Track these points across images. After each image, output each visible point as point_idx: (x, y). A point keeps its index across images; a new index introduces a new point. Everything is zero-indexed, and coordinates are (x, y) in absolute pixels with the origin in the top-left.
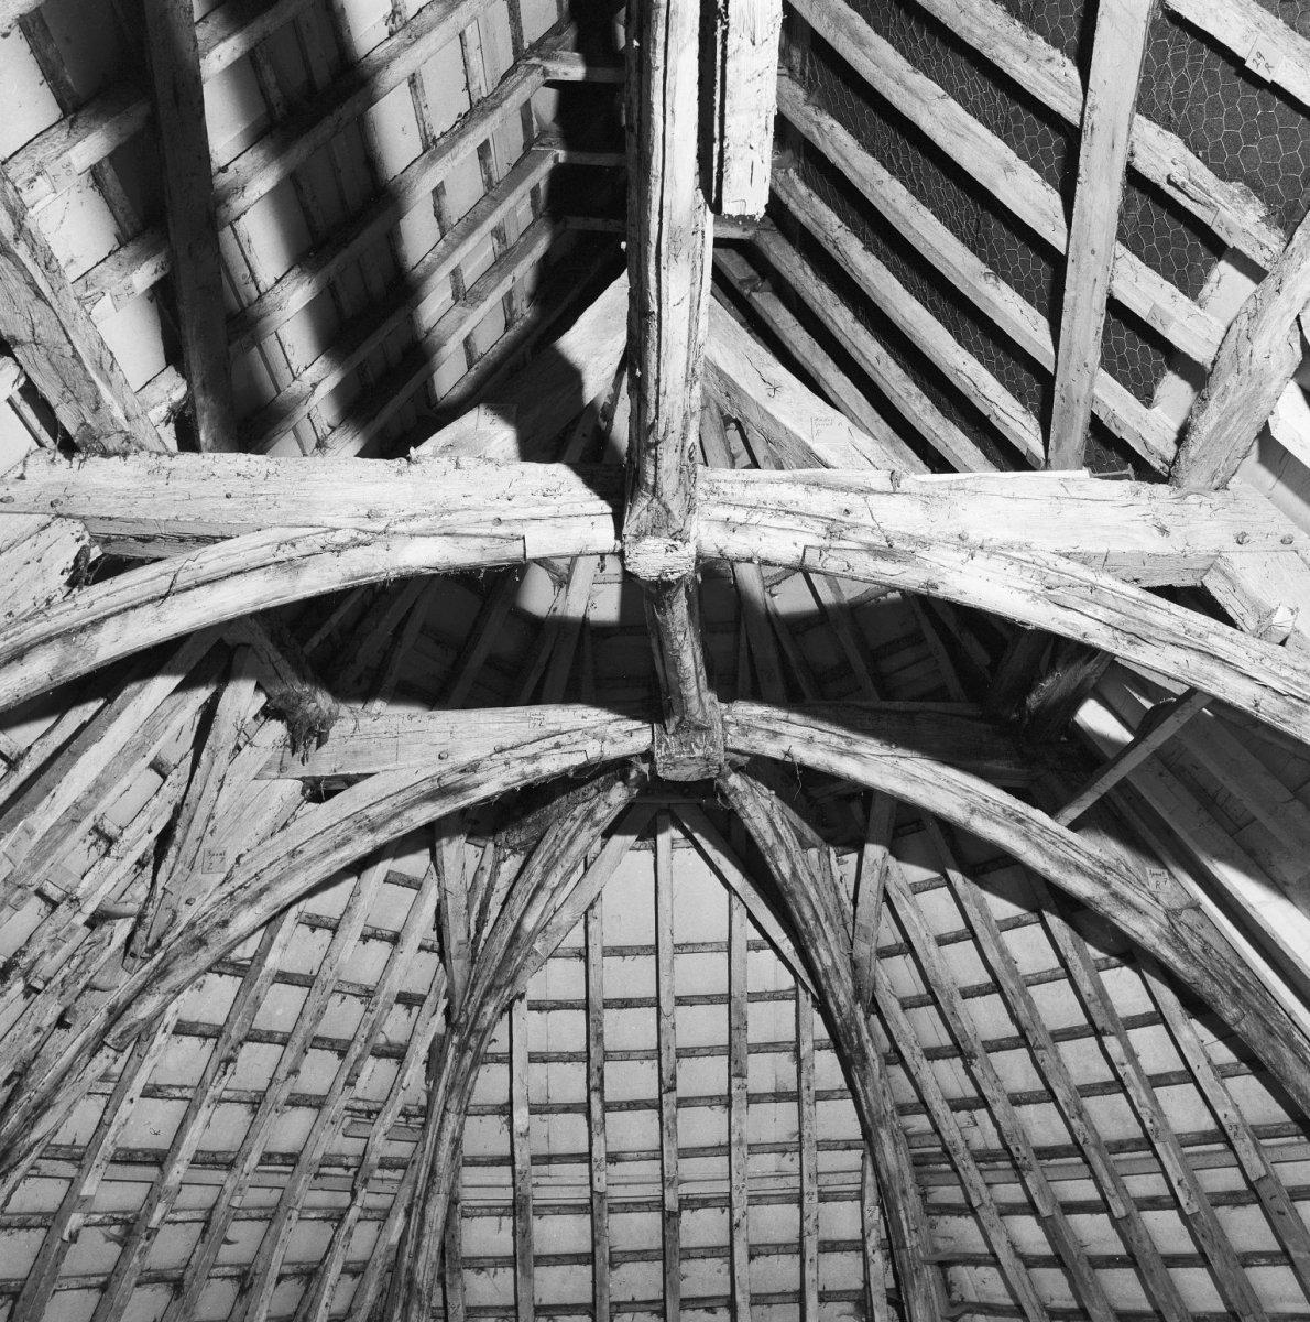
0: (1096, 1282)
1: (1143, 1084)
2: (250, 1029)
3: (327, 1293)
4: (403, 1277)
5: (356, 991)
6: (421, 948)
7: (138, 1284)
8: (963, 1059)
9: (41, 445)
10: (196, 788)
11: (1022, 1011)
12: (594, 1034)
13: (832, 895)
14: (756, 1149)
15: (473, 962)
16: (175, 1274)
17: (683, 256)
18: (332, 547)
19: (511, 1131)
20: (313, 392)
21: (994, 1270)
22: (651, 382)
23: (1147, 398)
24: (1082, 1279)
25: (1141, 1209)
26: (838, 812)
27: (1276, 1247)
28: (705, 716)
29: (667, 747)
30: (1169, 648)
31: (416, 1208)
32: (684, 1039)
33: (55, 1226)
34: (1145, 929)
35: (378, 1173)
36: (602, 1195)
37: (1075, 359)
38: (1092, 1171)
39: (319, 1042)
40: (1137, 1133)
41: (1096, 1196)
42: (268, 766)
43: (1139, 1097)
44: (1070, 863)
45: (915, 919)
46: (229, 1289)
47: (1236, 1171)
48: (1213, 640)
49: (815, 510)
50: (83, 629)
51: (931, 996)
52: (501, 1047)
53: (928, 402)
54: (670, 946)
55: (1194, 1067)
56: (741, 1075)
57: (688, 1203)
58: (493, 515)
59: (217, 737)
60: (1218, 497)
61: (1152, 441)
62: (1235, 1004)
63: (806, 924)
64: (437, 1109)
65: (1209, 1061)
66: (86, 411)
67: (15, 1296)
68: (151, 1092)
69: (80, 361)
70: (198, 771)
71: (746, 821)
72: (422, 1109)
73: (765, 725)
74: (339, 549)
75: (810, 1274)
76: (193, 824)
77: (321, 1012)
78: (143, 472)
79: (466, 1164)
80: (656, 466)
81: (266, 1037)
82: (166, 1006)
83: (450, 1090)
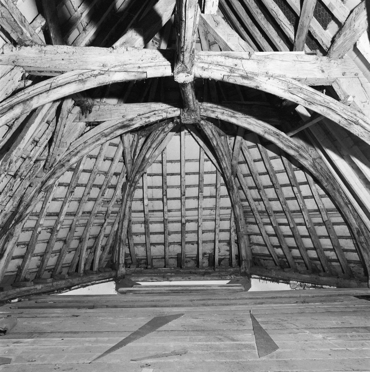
0: (285, 240)
1: (301, 198)
2: (77, 184)
3: (100, 242)
4: (118, 238)
5: (103, 173)
6: (119, 161)
7: (56, 241)
8: (258, 190)
9: (7, 42)
10: (58, 127)
11: (274, 179)
12: (164, 182)
13: (227, 148)
14: (205, 209)
15: (133, 165)
16: (64, 239)
17: (193, 6)
18: (94, 75)
19: (144, 205)
20: (81, 16)
21: (261, 237)
22: (183, 37)
23: (325, 27)
24: (281, 240)
25: (297, 225)
26: (230, 129)
27: (327, 235)
28: (195, 108)
29: (184, 116)
30: (319, 106)
31: (121, 222)
32: (187, 183)
33: (34, 230)
34: (306, 163)
35: (111, 215)
36: (167, 220)
37: (306, 14)
38: (287, 217)
39: (94, 186)
40: (299, 209)
41: (287, 222)
42: (76, 119)
43: (300, 201)
44: (290, 146)
45: (249, 156)
46: (78, 241)
47: (321, 218)
48: (331, 104)
49: (227, 64)
50: (28, 100)
51: (251, 174)
52: (140, 184)
53: (263, 16)
54: (184, 161)
55: (314, 195)
56: (202, 192)
57: (188, 221)
58: (138, 65)
59: (63, 115)
60: (340, 61)
61: (324, 41)
62: (326, 182)
63: (220, 156)
64: (125, 200)
65: (318, 194)
66: (19, 35)
67: (28, 245)
68: (54, 199)
69: (16, 22)
70: (58, 123)
71: (205, 132)
72: (121, 200)
73: (211, 109)
74: (95, 76)
75: (217, 237)
76: (58, 137)
77: (94, 179)
78: (37, 51)
79: (132, 212)
80: (183, 57)
81: (81, 185)
82: (56, 181)
83: (128, 196)
